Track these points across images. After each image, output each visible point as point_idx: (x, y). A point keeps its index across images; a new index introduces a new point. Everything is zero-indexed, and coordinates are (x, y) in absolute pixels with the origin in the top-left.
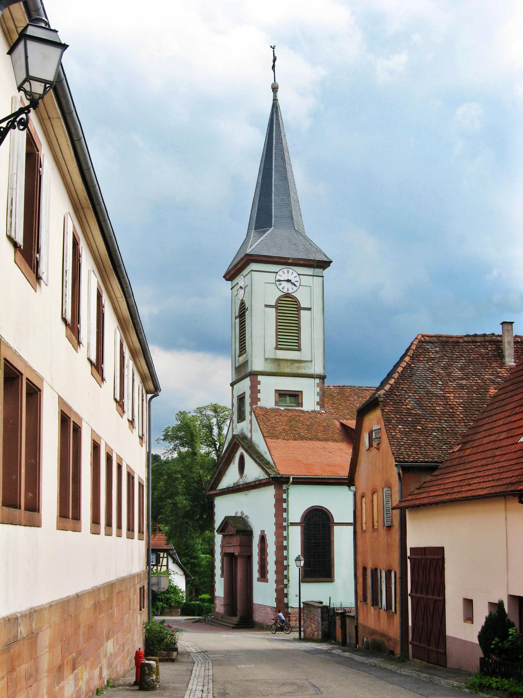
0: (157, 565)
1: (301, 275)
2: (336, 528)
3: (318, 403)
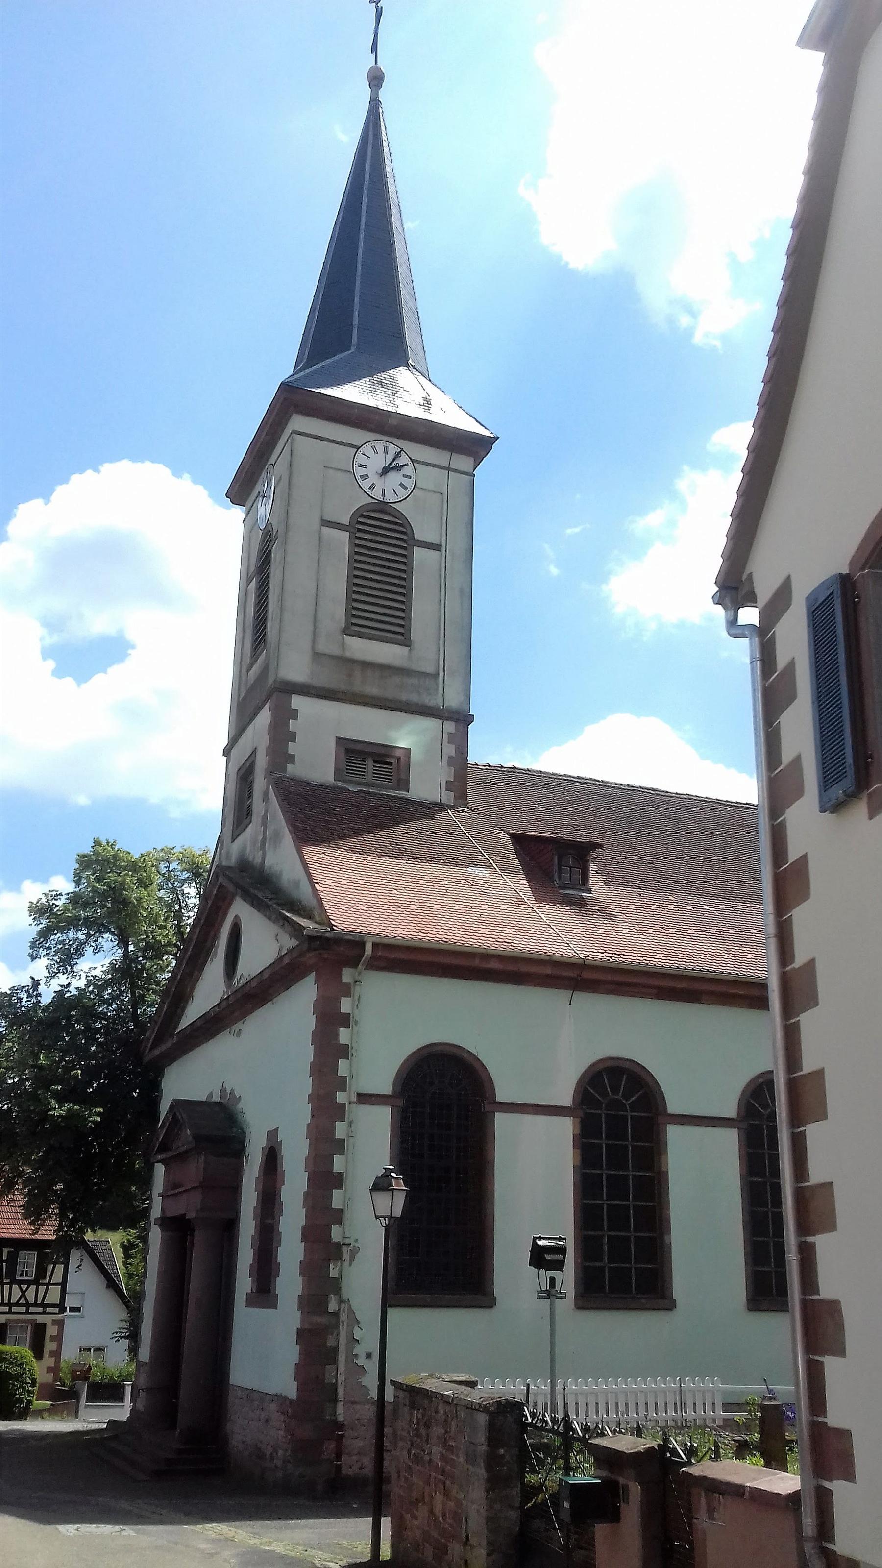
0: (36, 1282)
1: (419, 462)
2: (502, 1122)
3: (449, 786)
